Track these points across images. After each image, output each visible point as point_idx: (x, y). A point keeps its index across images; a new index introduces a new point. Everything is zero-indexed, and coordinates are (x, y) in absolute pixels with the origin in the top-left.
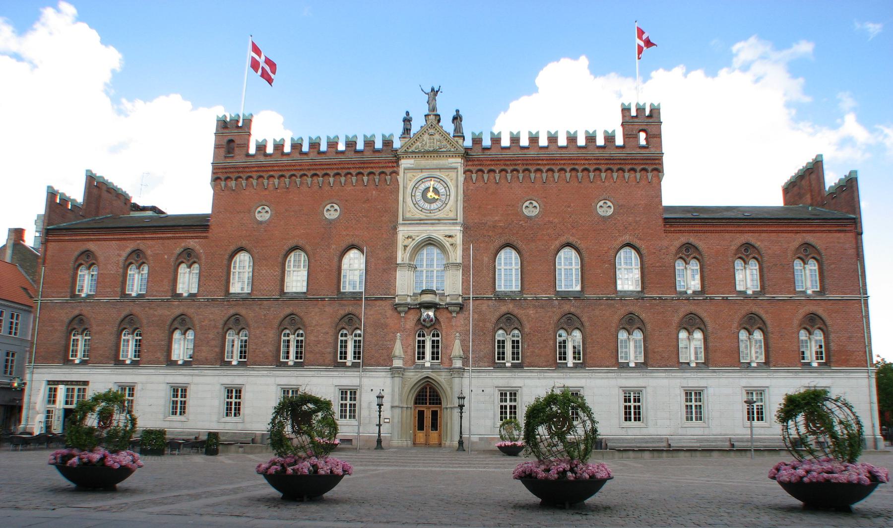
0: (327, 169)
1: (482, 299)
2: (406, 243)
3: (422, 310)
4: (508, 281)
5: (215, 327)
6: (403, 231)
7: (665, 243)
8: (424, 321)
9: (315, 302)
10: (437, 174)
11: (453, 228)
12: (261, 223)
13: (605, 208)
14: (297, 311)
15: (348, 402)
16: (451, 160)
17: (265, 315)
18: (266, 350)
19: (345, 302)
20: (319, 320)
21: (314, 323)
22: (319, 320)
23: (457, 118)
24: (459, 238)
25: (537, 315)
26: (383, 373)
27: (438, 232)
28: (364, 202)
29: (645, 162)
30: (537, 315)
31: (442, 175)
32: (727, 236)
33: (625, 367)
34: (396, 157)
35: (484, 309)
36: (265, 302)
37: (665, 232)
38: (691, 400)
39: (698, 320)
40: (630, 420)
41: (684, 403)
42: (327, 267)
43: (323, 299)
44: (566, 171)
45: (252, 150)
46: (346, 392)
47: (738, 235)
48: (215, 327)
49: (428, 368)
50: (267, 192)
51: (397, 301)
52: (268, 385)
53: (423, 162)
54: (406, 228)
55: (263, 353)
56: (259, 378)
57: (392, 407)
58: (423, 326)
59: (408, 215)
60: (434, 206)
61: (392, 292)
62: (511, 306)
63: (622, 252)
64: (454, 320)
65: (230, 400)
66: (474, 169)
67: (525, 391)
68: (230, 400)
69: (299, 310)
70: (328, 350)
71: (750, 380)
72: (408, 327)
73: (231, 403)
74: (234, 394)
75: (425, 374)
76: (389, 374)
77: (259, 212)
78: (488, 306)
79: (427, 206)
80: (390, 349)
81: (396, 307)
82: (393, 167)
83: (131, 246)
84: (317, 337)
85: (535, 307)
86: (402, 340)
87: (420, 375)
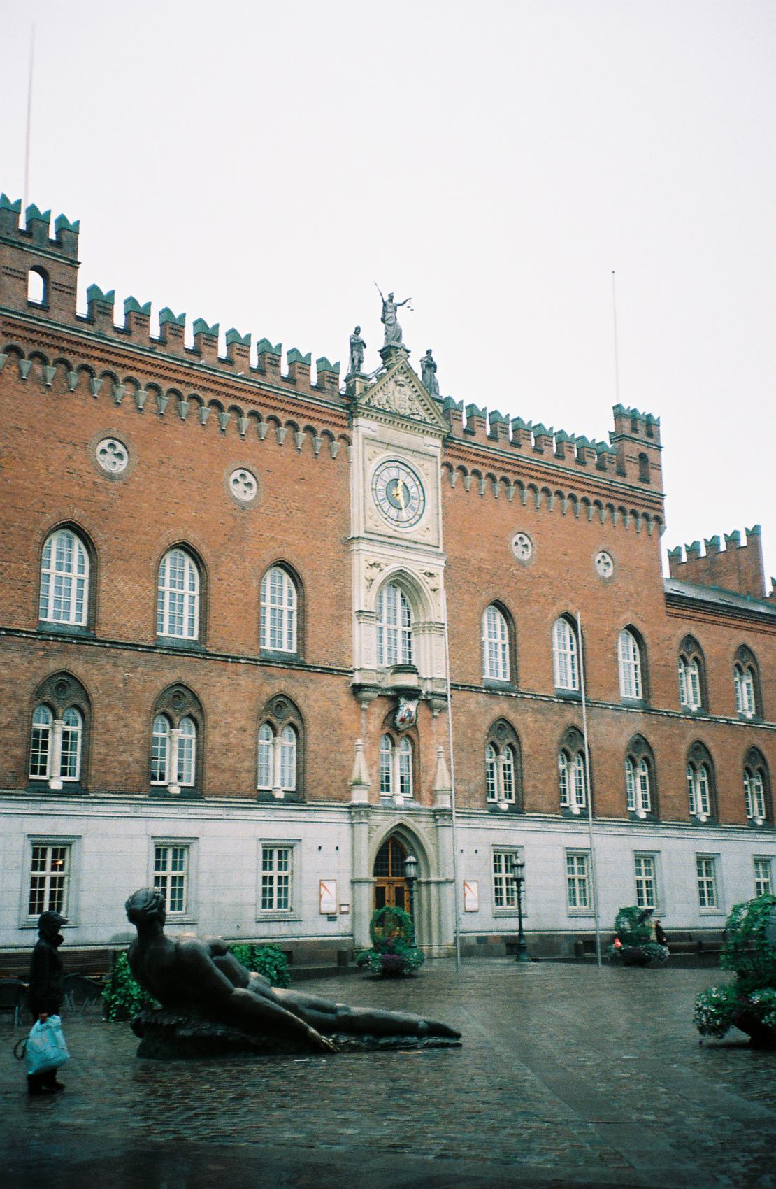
3: (402, 701)
4: (176, 619)
5: (14, 697)
7: (668, 630)
8: (403, 720)
9: (221, 665)
10: (408, 458)
11: (435, 561)
13: (109, 457)
14: (189, 679)
15: (48, 874)
16: (429, 440)
17: (125, 682)
18: (125, 757)
21: (221, 707)
24: (439, 581)
25: (537, 725)
26: (338, 815)
27: (417, 565)
28: (297, 482)
30: (537, 725)
33: (266, 798)
34: (351, 405)
35: (472, 707)
36: (126, 653)
37: (669, 614)
38: (43, 863)
39: (189, 699)
42: (241, 596)
43: (236, 660)
44: (69, 368)
46: (44, 851)
47: (736, 631)
48: (14, 697)
50: (120, 413)
51: (357, 679)
52: (132, 837)
54: (370, 548)
55: (120, 763)
56: (113, 822)
57: (353, 882)
59: (370, 524)
63: (168, 557)
64: (434, 722)
65: (38, 874)
66: (456, 463)
68: (38, 874)
70: (247, 764)
72: (371, 728)
73: (43, 880)
74: (508, 862)
76: (344, 818)
77: (104, 451)
78: (478, 703)
80: (346, 769)
82: (344, 427)
83: (745, 637)
84: (226, 735)
85: (534, 711)
87: (392, 819)
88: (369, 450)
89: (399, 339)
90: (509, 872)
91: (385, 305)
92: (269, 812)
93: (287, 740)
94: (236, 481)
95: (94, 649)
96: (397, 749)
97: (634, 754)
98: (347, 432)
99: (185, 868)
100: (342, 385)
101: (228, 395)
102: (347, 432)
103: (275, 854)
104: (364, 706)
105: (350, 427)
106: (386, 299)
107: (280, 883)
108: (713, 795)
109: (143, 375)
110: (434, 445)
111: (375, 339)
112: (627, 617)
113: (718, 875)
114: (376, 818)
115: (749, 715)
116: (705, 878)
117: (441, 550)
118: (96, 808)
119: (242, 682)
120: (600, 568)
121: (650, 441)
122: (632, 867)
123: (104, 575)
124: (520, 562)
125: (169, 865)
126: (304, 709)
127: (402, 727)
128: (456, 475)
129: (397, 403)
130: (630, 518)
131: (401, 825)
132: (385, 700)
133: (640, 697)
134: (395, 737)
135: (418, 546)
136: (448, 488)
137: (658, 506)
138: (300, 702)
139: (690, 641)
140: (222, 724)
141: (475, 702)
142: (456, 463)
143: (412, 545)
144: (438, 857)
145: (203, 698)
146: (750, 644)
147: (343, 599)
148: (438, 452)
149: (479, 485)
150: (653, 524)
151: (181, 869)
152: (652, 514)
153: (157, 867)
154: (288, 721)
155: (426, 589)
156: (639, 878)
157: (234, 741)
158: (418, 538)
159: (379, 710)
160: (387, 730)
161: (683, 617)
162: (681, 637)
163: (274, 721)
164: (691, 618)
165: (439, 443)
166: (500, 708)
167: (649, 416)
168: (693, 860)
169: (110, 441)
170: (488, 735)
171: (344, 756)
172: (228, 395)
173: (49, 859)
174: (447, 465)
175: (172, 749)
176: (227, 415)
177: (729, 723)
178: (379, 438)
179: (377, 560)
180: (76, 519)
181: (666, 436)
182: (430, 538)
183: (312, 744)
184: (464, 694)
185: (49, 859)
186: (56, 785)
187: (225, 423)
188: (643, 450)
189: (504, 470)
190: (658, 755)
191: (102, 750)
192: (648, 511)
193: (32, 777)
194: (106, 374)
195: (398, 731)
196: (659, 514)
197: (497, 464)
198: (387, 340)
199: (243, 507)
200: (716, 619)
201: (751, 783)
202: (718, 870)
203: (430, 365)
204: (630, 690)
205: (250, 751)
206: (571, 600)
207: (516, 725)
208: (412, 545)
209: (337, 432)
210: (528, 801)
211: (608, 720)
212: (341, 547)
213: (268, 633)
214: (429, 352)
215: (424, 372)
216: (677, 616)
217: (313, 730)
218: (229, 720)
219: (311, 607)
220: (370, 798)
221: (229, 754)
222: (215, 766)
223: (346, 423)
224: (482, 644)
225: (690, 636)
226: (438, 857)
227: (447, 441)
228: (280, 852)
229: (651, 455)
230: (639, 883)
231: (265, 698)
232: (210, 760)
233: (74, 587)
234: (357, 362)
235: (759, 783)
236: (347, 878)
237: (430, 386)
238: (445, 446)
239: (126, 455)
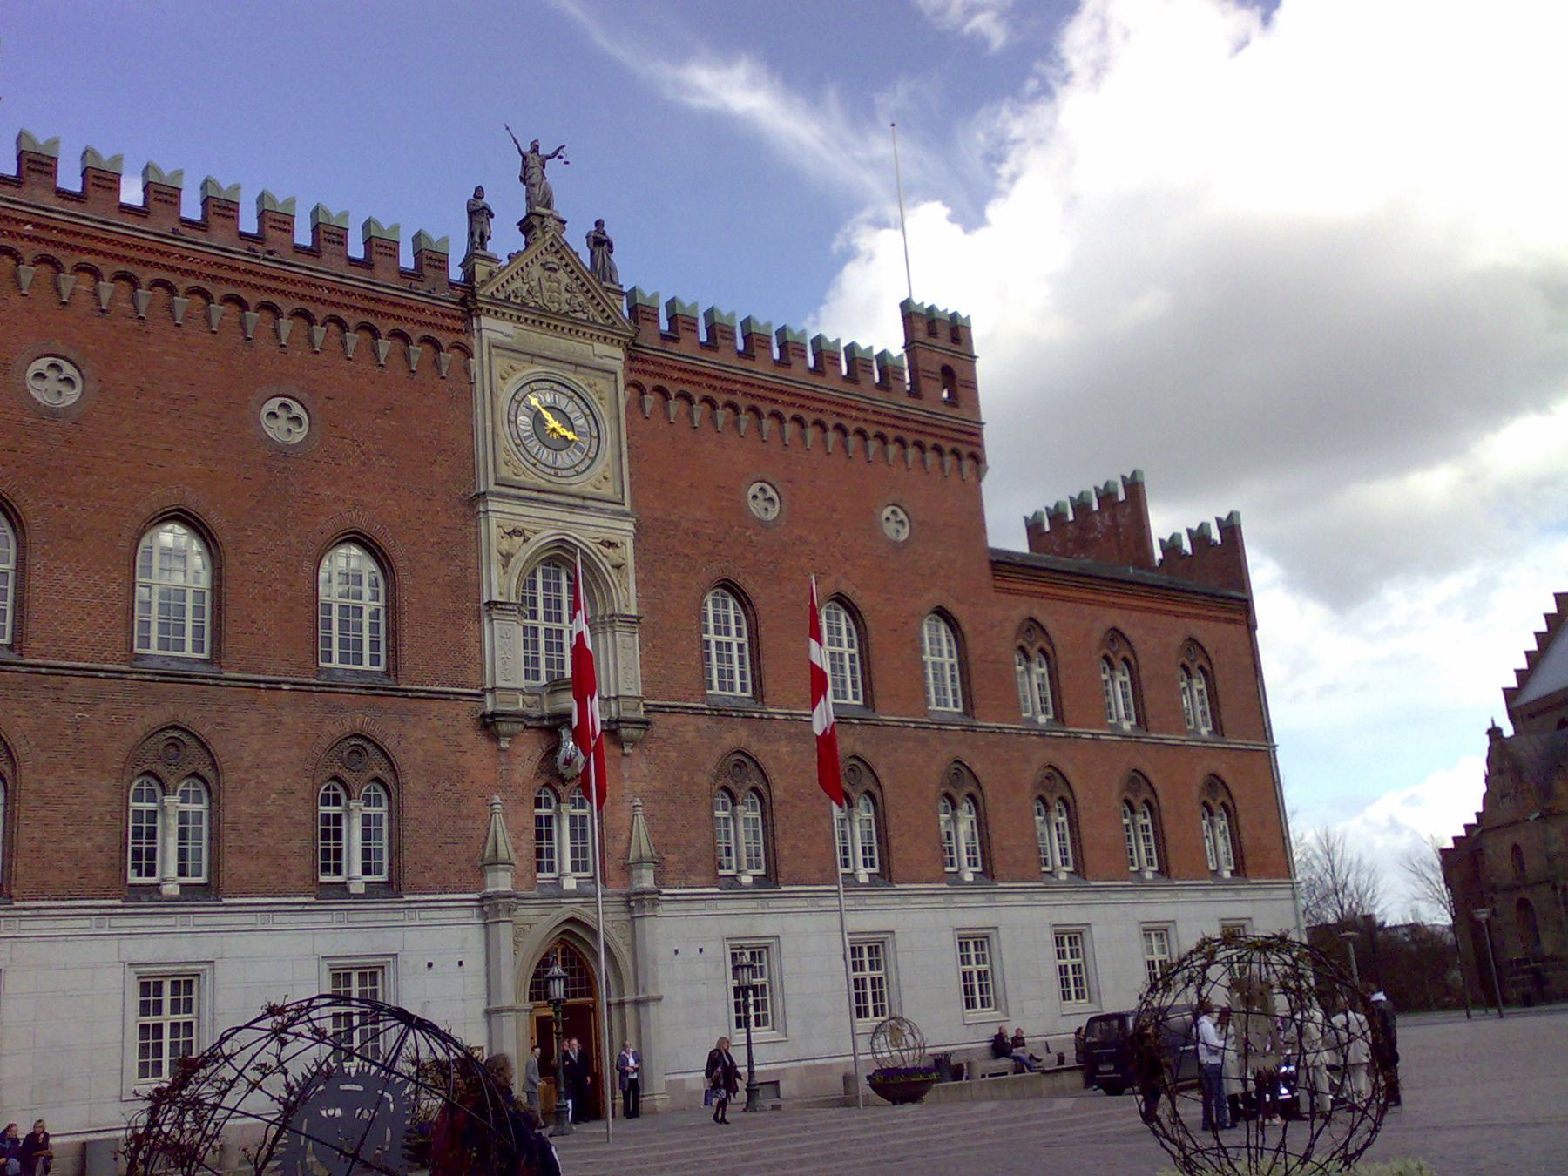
0: (58, 245)
1: (685, 710)
2: (505, 545)
6: (499, 515)
9: (248, 694)
12: (52, 413)
14: (188, 717)
15: (167, 1018)
16: (601, 348)
19: (344, 699)
20: (269, 753)
22: (269, 753)
23: (600, 241)
24: (628, 553)
27: (587, 530)
29: (371, 305)
31: (578, 379)
32: (1087, 609)
34: (468, 302)
36: (78, 682)
37: (997, 590)
38: (158, 1005)
40: (974, 1006)
41: (134, 1020)
43: (273, 686)
45: (1158, 554)
46: (159, 986)
49: (570, 894)
51: (489, 705)
53: (537, 339)
54: (506, 508)
57: (489, 1013)
58: (552, 775)
59: (505, 472)
60: (564, 459)
61: (473, 678)
62: (743, 732)
65: (181, 1018)
67: (1182, 928)
68: (181, 1018)
69: (197, 713)
70: (296, 844)
71: (1150, 908)
75: (566, 912)
77: (273, 414)
78: (698, 730)
79: (546, 455)
81: (488, 724)
83: (1115, 618)
86: (505, 815)
87: (555, 912)
88: (500, 364)
89: (548, 205)
90: (869, 974)
91: (525, 158)
92: (341, 916)
93: (750, 812)
94: (755, 497)
95: (21, 678)
96: (855, 810)
97: (952, 791)
98: (462, 338)
99: (195, 1009)
100: (456, 274)
101: (256, 288)
102: (462, 338)
103: (865, 950)
104: (504, 745)
105: (469, 331)
106: (526, 148)
107: (873, 986)
108: (1077, 842)
109: (108, 261)
110: (613, 356)
111: (509, 206)
112: (936, 597)
113: (892, 969)
114: (528, 913)
115: (1127, 726)
116: (973, 967)
117: (627, 508)
118: (27, 924)
119: (285, 719)
120: (890, 529)
121: (957, 348)
122: (953, 953)
123: (37, 563)
124: (763, 524)
125: (166, 1006)
126: (400, 759)
127: (568, 773)
128: (650, 400)
129: (546, 294)
130: (931, 457)
131: (571, 920)
132: (541, 735)
133: (960, 710)
134: (560, 788)
135: (589, 503)
136: (640, 419)
137: (974, 439)
138: (390, 744)
139: (1032, 625)
140: (252, 784)
141: (690, 728)
142: (649, 382)
143: (578, 502)
144: (635, 964)
145: (217, 746)
146: (1122, 627)
147: (466, 584)
148: (619, 366)
149: (690, 415)
150: (967, 464)
151: (189, 1011)
152: (965, 450)
153: (144, 1009)
154: (370, 774)
155: (605, 565)
156: (967, 968)
157: (273, 810)
158: (589, 490)
159: (526, 753)
160: (545, 778)
161: (1019, 593)
162: (1018, 621)
163: (346, 776)
164: (1032, 594)
165: (619, 352)
166: (736, 736)
167: (954, 316)
168: (1049, 937)
169: (759, 485)
170: (717, 778)
171: (470, 823)
172: (256, 288)
173: (167, 997)
174: (631, 384)
175: (165, 826)
176: (252, 316)
177: (1095, 738)
178: (515, 347)
179: (520, 525)
180: (362, 526)
181: (978, 334)
182: (608, 491)
183: (413, 809)
184: (675, 719)
185: (167, 997)
186: (357, 888)
187: (250, 328)
188: (946, 361)
189: (879, 423)
190: (987, 789)
191: (37, 834)
192: (959, 446)
193: (323, 879)
194: (363, 327)
195: (563, 780)
196: (975, 449)
197: (717, 383)
198: (530, 205)
199: (284, 452)
200: (1084, 595)
201: (1134, 822)
202: (1088, 949)
203: (600, 241)
204: (944, 701)
205: (299, 824)
206: (845, 575)
207: (761, 759)
208: (578, 502)
209: (445, 339)
210: (408, 877)
211: (910, 744)
212: (461, 510)
213: (932, 690)
214: (599, 224)
215: (592, 253)
216: (1009, 592)
217: (414, 785)
218: (265, 778)
219: (407, 600)
220: (516, 883)
221: (265, 830)
222: (241, 850)
223: (462, 326)
224: (924, 664)
225: (1115, 630)
226: (635, 964)
227: (634, 353)
228: (870, 948)
229: (957, 367)
230: (967, 977)
231: (325, 742)
232: (230, 840)
233: (735, 653)
234: (479, 238)
235: (1147, 821)
236: (481, 1006)
237: (603, 271)
238: (631, 358)
239: (78, 381)
